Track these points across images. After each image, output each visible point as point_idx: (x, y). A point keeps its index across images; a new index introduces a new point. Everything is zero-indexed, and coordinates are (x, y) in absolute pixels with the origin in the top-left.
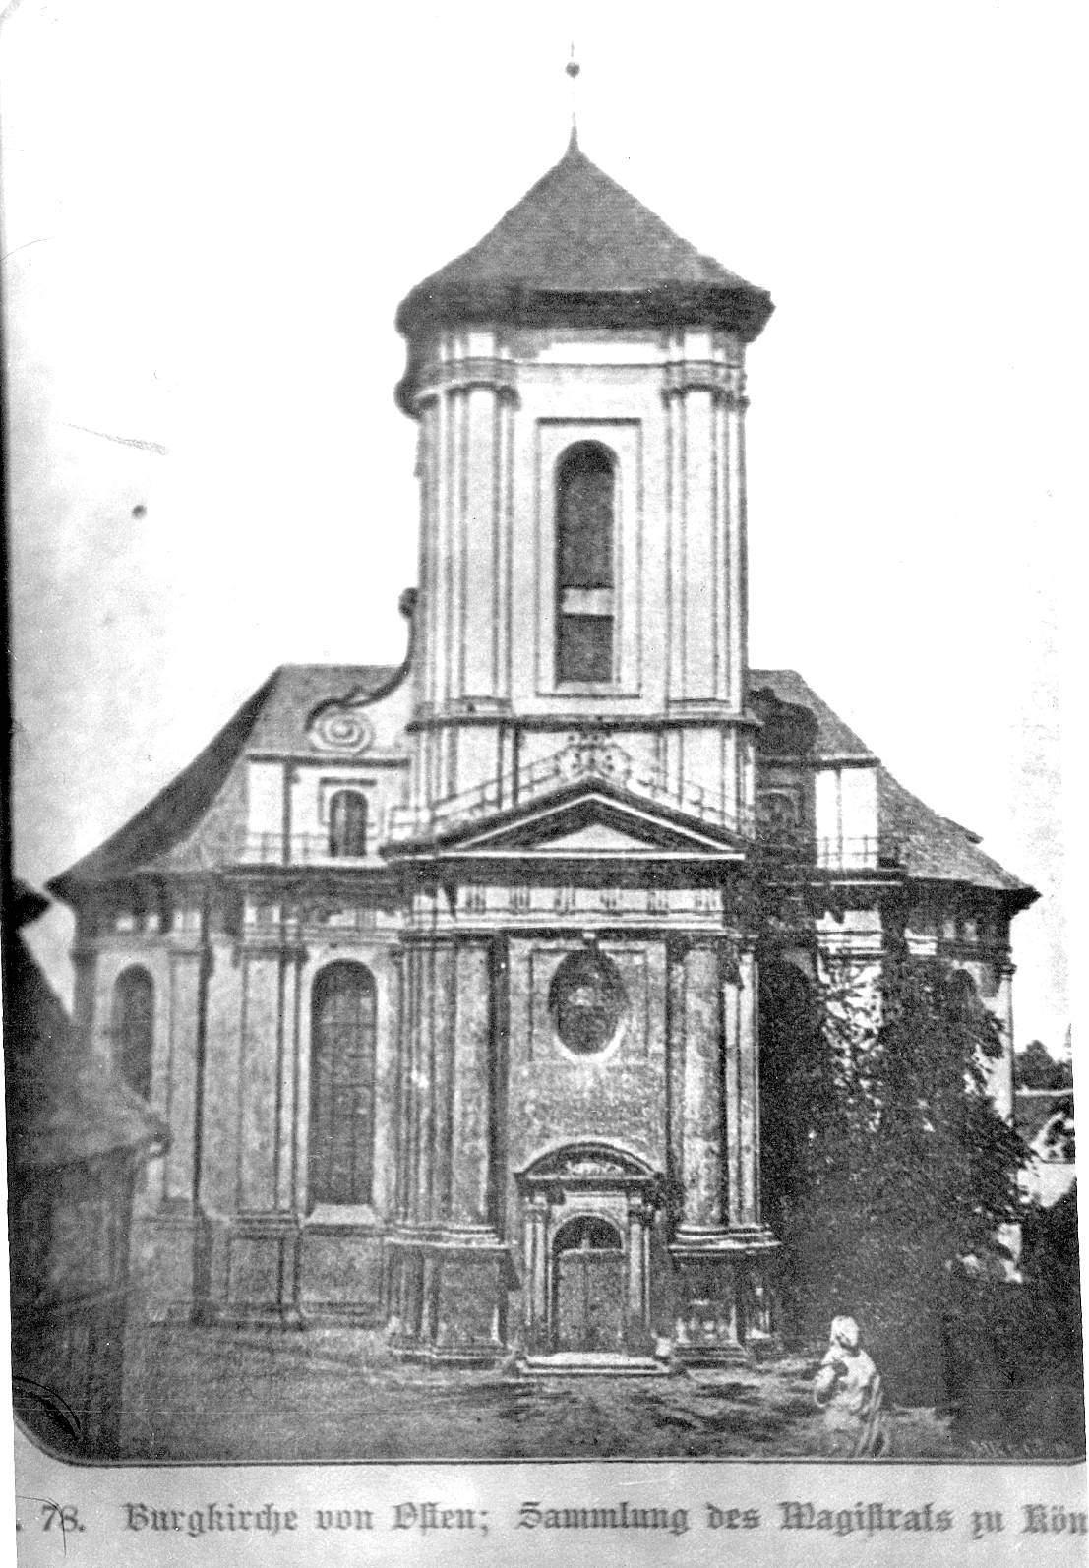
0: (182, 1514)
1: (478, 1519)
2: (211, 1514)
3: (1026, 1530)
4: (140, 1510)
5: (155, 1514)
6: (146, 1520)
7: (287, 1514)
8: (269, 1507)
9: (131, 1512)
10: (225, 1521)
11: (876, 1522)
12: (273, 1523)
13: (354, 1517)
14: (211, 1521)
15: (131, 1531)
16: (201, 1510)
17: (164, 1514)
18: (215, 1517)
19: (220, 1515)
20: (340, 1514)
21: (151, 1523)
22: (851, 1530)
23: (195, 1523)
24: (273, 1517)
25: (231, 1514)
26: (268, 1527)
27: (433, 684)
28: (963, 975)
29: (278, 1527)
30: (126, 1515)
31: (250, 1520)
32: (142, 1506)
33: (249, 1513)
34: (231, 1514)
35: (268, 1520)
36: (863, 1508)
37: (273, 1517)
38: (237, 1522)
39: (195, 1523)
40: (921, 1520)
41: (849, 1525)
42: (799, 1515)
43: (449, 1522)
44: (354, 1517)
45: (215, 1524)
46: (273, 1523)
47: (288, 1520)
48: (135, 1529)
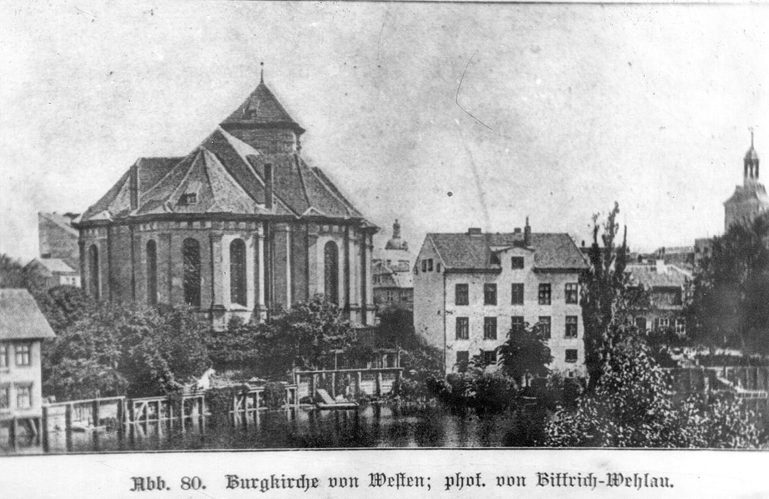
0: (575, 478)
1: (426, 482)
2: (272, 481)
3: (227, 487)
5: (242, 480)
6: (547, 480)
7: (313, 480)
8: (590, 475)
9: (540, 477)
10: (280, 483)
11: (400, 483)
12: (306, 484)
13: (516, 480)
14: (272, 484)
15: (540, 486)
16: (267, 478)
17: (247, 480)
18: (275, 482)
19: (277, 480)
20: (468, 479)
21: (240, 485)
22: (268, 489)
23: (264, 485)
24: (306, 482)
25: (283, 480)
26: (590, 485)
27: (356, 275)
28: (716, 389)
29: (640, 486)
30: (227, 481)
31: (294, 483)
33: (293, 480)
34: (283, 480)
35: (590, 481)
36: (285, 478)
37: (306, 482)
38: (568, 481)
39: (264, 485)
40: (475, 480)
41: (267, 486)
42: (615, 480)
43: (392, 484)
44: (516, 480)
45: (275, 485)
46: (306, 484)
47: (409, 482)
48: (542, 485)
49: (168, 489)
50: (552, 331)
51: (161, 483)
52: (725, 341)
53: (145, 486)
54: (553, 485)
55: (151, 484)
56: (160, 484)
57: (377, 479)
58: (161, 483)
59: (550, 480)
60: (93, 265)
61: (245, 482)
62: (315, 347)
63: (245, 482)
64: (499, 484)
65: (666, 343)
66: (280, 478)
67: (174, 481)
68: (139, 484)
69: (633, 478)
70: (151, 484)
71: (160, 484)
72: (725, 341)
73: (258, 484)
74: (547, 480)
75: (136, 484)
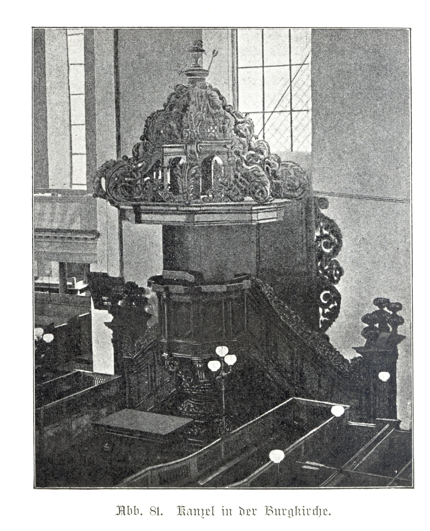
4: (270, 508)
5: (276, 509)
6: (272, 512)
10: (301, 512)
18: (298, 511)
31: (311, 512)
32: (271, 507)
34: (304, 510)
43: (249, 514)
49: (141, 514)
50: (84, 73)
51: (137, 511)
52: (320, 327)
53: (126, 512)
54: (276, 514)
55: (130, 511)
56: (136, 511)
57: (269, 510)
58: (137, 511)
59: (274, 511)
60: (164, 176)
61: (278, 511)
62: (53, 195)
63: (278, 511)
64: (240, 514)
65: (194, 186)
66: (301, 508)
67: (144, 509)
68: (121, 510)
69: (211, 510)
70: (130, 511)
71: (136, 511)
72: (320, 327)
73: (286, 512)
74: (272, 512)
75: (120, 511)
